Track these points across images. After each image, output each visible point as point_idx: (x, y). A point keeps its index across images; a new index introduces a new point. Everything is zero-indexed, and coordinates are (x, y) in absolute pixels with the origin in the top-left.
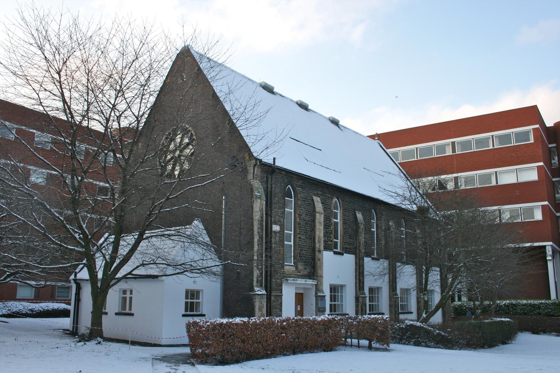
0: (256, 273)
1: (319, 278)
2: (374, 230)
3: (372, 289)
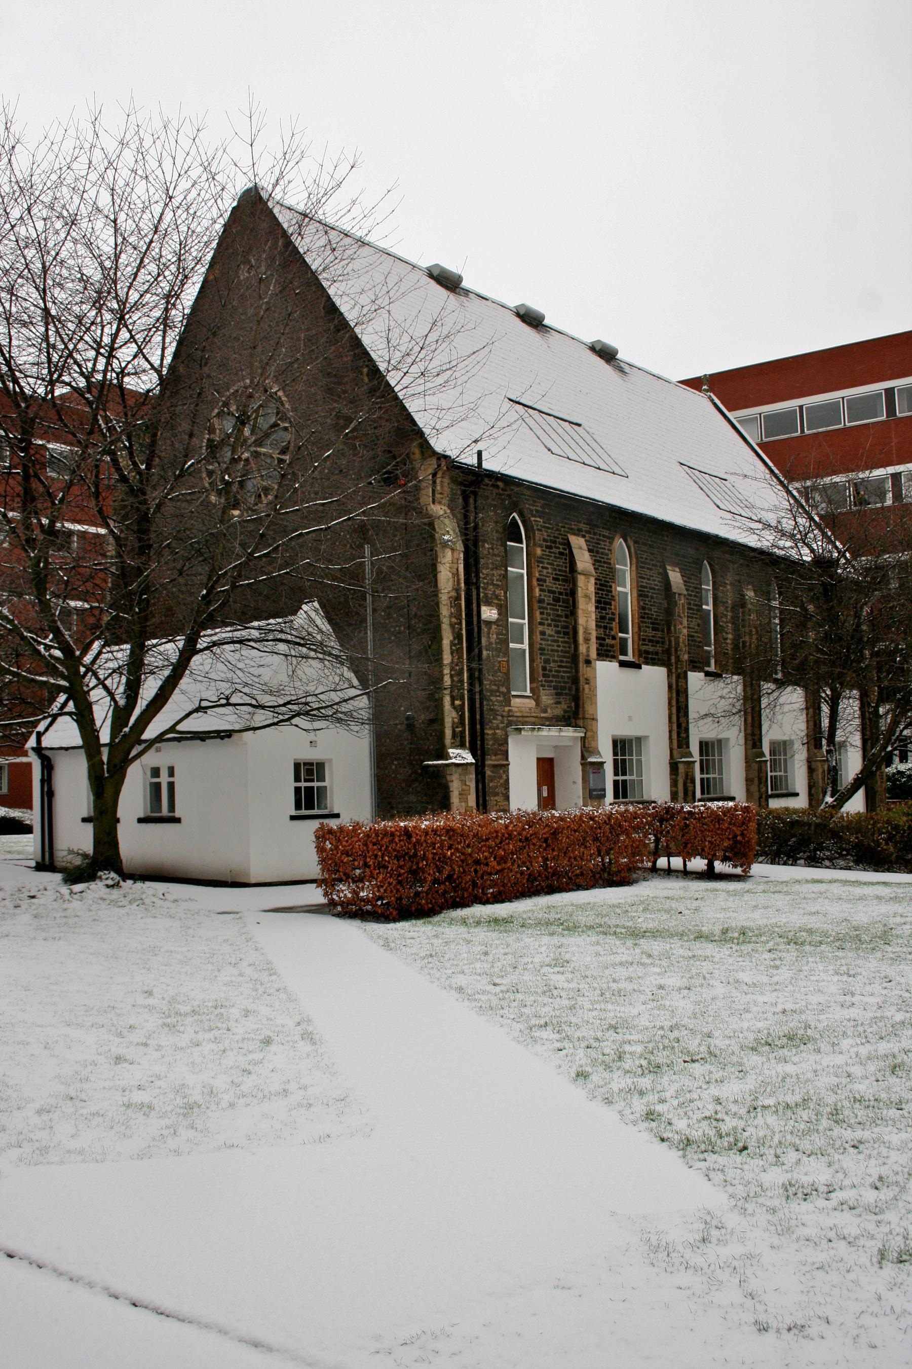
0: (450, 716)
1: (589, 722)
2: (709, 607)
3: (707, 743)
